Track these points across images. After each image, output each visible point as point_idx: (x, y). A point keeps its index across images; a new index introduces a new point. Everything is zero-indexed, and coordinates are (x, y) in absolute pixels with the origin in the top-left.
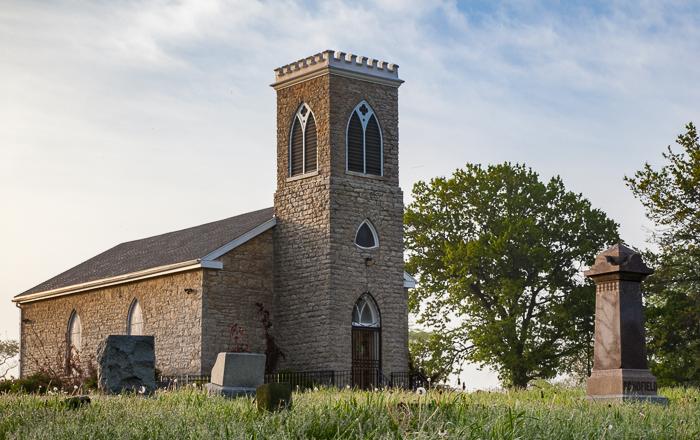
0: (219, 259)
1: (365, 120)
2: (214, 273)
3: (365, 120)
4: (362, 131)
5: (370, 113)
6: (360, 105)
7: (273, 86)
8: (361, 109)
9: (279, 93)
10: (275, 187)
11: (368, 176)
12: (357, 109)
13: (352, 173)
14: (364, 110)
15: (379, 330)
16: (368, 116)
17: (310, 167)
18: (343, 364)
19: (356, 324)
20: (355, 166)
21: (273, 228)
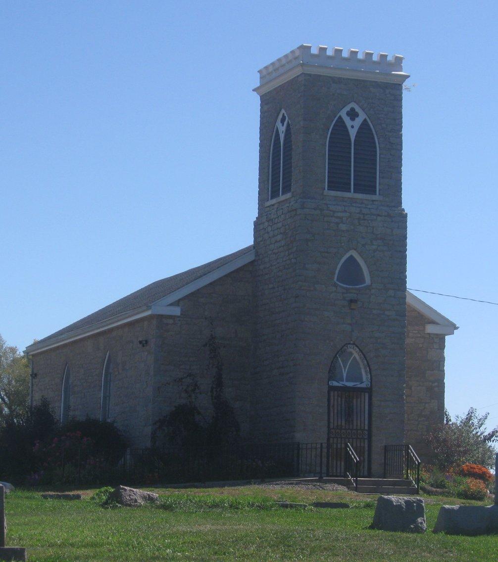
0: (176, 303)
1: (353, 128)
2: (171, 321)
3: (353, 128)
4: (350, 140)
5: (362, 116)
6: (347, 108)
7: (253, 90)
8: (348, 114)
9: (262, 98)
10: (255, 214)
11: (359, 196)
12: (343, 113)
13: (333, 193)
14: (353, 115)
15: (369, 390)
16: (358, 122)
17: (287, 189)
18: (366, 473)
19: (335, 384)
20: (338, 182)
21: (252, 263)
